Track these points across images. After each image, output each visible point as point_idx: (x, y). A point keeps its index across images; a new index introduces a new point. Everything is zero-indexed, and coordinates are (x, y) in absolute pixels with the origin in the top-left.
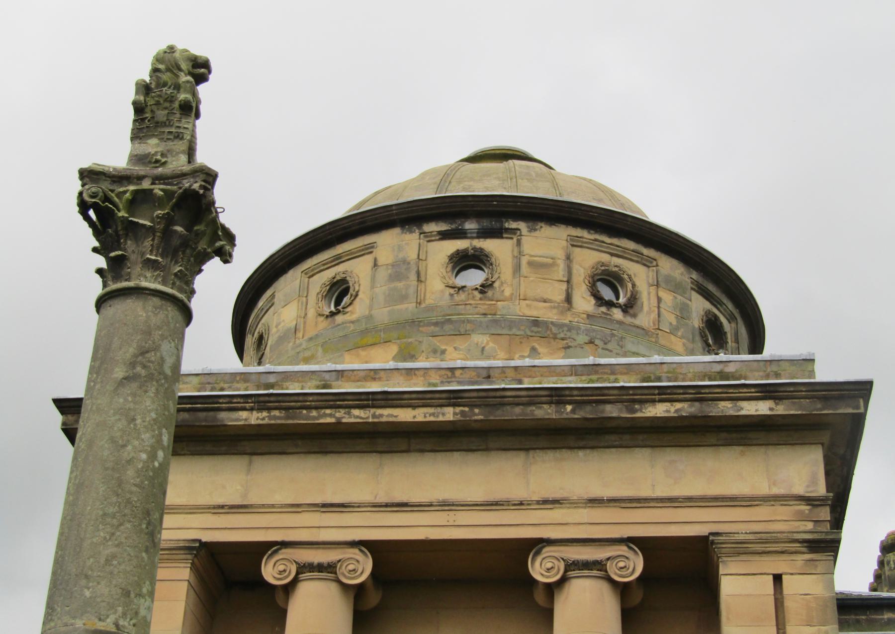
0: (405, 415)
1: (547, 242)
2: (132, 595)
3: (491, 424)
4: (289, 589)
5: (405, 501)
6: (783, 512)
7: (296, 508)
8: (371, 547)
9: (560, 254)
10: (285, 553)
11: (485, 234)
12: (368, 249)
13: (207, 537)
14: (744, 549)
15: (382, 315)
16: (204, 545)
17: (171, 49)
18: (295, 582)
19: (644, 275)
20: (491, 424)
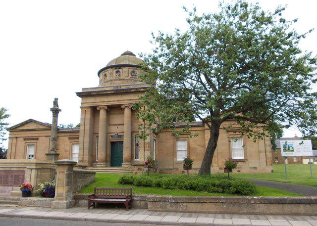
0: (109, 92)
3: (117, 92)
8: (108, 106)
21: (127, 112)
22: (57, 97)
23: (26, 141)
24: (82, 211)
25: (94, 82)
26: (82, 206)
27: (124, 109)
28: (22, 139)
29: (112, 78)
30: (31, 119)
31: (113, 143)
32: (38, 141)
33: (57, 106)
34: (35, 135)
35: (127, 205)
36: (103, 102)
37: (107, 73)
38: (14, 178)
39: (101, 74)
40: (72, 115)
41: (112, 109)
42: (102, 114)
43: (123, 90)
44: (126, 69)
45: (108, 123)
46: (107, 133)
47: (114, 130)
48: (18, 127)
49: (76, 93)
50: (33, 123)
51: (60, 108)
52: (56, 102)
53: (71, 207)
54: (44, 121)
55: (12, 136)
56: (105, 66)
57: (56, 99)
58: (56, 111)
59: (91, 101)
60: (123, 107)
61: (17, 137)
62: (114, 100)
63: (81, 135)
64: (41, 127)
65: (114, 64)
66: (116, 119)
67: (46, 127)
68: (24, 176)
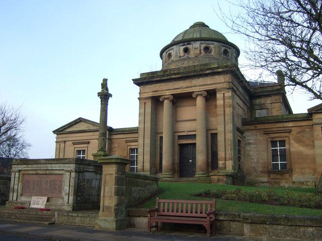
2: (8, 142)
6: (225, 84)
8: (172, 95)
9: (199, 46)
11: (188, 44)
12: (173, 49)
14: (220, 90)
15: (175, 59)
16: (154, 97)
19: (213, 46)
21: (200, 101)
24: (163, 118)
25: (156, 65)
26: (106, 91)
28: (71, 142)
30: (80, 118)
31: (182, 146)
32: (89, 145)
33: (107, 89)
34: (86, 138)
36: (167, 90)
38: (48, 185)
39: (164, 54)
40: (126, 113)
41: (179, 99)
42: (167, 104)
44: (197, 45)
45: (175, 120)
46: (174, 131)
47: (185, 128)
48: (67, 128)
49: (133, 80)
50: (83, 123)
51: (110, 92)
53: (78, 210)
55: (60, 140)
56: (169, 42)
57: (105, 81)
58: (105, 96)
59: (150, 90)
60: (194, 96)
61: (65, 142)
62: (182, 87)
64: (92, 128)
65: (180, 38)
67: (98, 128)
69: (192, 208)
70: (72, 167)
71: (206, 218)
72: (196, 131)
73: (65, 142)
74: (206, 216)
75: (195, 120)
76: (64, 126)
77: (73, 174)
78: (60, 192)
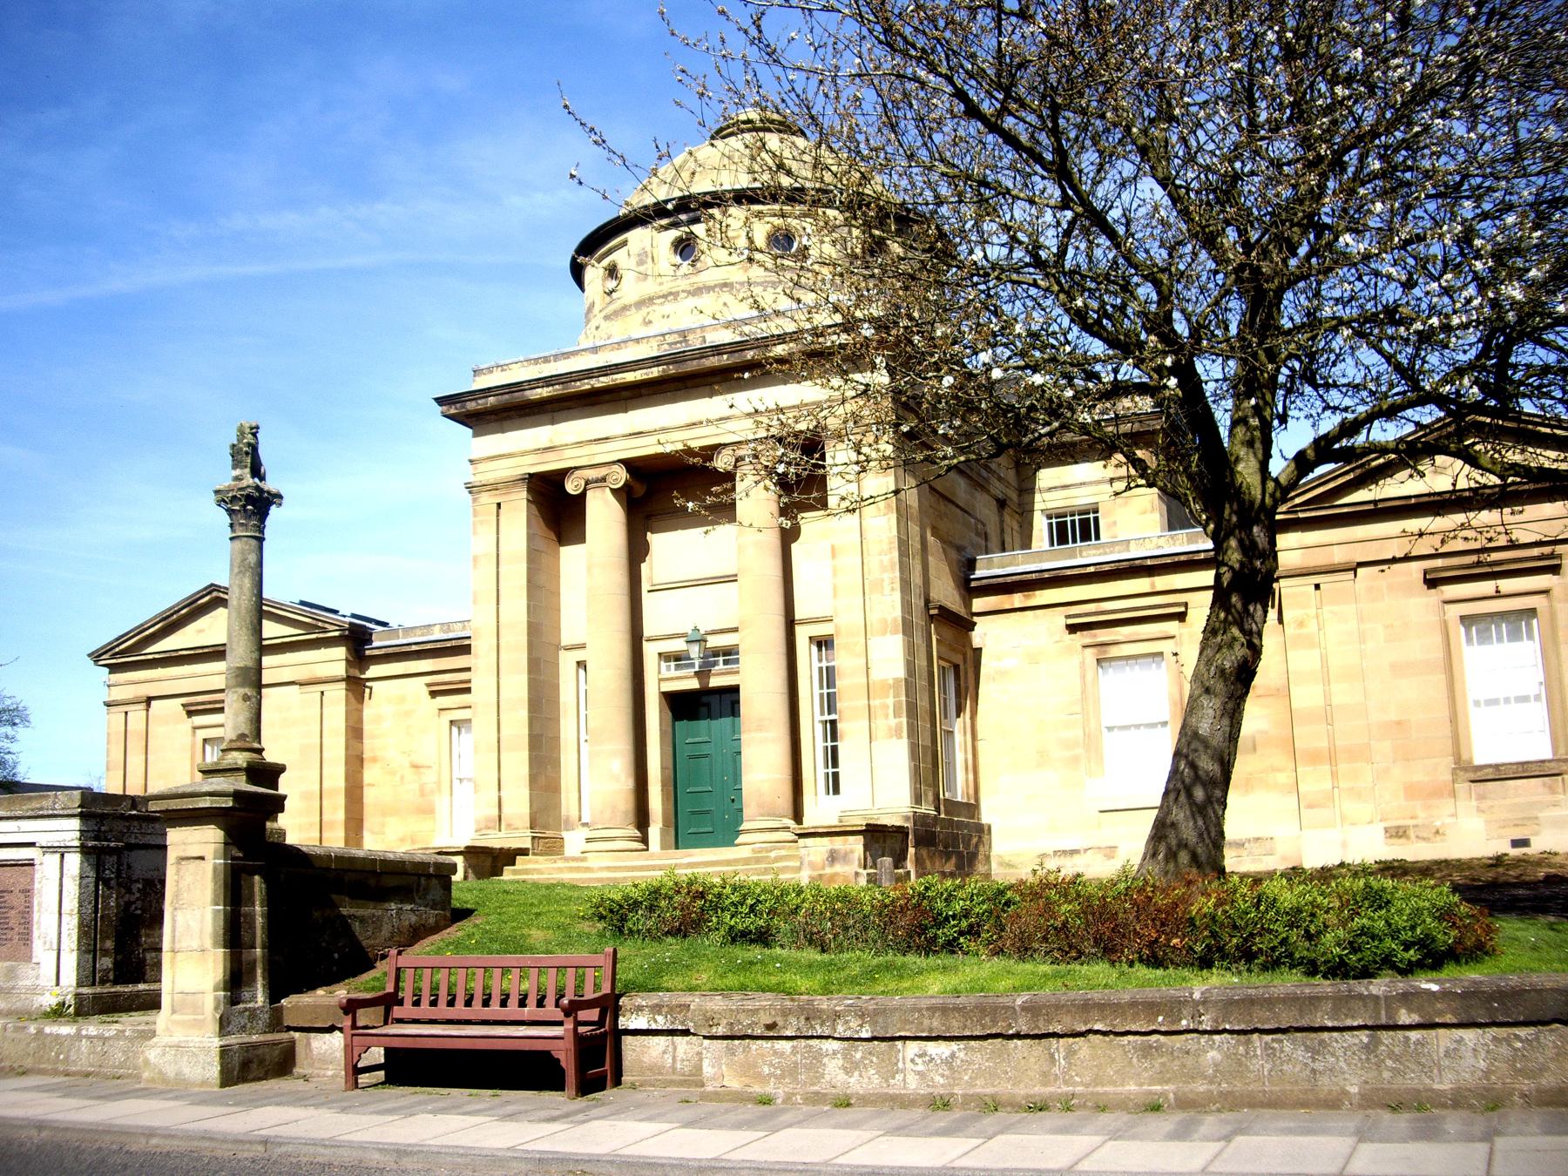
0: (630, 377)
1: (638, 237)
3: (686, 377)
4: (583, 495)
5: (980, 736)
7: (580, 444)
8: (628, 464)
10: (578, 473)
13: (532, 471)
17: (475, 435)
18: (585, 490)
20: (686, 377)
21: (756, 501)
22: (248, 422)
23: (199, 720)
27: (729, 477)
29: (650, 288)
35: (595, 1065)
37: (619, 257)
43: (718, 350)
52: (248, 455)
54: (1226, 829)
61: (149, 700)
63: (480, 661)
66: (672, 550)
68: (28, 892)
69: (435, 989)
70: (69, 830)
71: (560, 1023)
72: (735, 630)
73: (149, 700)
74: (560, 1016)
75: (732, 579)
76: (141, 629)
77: (74, 861)
78: (26, 938)
